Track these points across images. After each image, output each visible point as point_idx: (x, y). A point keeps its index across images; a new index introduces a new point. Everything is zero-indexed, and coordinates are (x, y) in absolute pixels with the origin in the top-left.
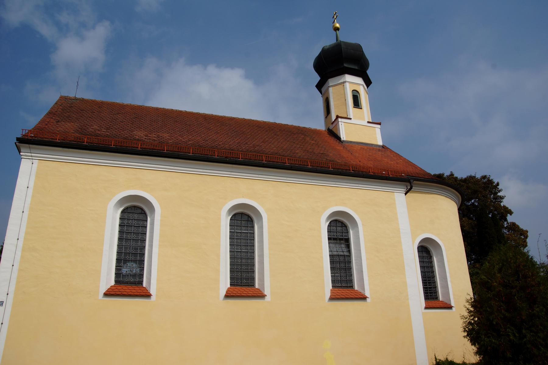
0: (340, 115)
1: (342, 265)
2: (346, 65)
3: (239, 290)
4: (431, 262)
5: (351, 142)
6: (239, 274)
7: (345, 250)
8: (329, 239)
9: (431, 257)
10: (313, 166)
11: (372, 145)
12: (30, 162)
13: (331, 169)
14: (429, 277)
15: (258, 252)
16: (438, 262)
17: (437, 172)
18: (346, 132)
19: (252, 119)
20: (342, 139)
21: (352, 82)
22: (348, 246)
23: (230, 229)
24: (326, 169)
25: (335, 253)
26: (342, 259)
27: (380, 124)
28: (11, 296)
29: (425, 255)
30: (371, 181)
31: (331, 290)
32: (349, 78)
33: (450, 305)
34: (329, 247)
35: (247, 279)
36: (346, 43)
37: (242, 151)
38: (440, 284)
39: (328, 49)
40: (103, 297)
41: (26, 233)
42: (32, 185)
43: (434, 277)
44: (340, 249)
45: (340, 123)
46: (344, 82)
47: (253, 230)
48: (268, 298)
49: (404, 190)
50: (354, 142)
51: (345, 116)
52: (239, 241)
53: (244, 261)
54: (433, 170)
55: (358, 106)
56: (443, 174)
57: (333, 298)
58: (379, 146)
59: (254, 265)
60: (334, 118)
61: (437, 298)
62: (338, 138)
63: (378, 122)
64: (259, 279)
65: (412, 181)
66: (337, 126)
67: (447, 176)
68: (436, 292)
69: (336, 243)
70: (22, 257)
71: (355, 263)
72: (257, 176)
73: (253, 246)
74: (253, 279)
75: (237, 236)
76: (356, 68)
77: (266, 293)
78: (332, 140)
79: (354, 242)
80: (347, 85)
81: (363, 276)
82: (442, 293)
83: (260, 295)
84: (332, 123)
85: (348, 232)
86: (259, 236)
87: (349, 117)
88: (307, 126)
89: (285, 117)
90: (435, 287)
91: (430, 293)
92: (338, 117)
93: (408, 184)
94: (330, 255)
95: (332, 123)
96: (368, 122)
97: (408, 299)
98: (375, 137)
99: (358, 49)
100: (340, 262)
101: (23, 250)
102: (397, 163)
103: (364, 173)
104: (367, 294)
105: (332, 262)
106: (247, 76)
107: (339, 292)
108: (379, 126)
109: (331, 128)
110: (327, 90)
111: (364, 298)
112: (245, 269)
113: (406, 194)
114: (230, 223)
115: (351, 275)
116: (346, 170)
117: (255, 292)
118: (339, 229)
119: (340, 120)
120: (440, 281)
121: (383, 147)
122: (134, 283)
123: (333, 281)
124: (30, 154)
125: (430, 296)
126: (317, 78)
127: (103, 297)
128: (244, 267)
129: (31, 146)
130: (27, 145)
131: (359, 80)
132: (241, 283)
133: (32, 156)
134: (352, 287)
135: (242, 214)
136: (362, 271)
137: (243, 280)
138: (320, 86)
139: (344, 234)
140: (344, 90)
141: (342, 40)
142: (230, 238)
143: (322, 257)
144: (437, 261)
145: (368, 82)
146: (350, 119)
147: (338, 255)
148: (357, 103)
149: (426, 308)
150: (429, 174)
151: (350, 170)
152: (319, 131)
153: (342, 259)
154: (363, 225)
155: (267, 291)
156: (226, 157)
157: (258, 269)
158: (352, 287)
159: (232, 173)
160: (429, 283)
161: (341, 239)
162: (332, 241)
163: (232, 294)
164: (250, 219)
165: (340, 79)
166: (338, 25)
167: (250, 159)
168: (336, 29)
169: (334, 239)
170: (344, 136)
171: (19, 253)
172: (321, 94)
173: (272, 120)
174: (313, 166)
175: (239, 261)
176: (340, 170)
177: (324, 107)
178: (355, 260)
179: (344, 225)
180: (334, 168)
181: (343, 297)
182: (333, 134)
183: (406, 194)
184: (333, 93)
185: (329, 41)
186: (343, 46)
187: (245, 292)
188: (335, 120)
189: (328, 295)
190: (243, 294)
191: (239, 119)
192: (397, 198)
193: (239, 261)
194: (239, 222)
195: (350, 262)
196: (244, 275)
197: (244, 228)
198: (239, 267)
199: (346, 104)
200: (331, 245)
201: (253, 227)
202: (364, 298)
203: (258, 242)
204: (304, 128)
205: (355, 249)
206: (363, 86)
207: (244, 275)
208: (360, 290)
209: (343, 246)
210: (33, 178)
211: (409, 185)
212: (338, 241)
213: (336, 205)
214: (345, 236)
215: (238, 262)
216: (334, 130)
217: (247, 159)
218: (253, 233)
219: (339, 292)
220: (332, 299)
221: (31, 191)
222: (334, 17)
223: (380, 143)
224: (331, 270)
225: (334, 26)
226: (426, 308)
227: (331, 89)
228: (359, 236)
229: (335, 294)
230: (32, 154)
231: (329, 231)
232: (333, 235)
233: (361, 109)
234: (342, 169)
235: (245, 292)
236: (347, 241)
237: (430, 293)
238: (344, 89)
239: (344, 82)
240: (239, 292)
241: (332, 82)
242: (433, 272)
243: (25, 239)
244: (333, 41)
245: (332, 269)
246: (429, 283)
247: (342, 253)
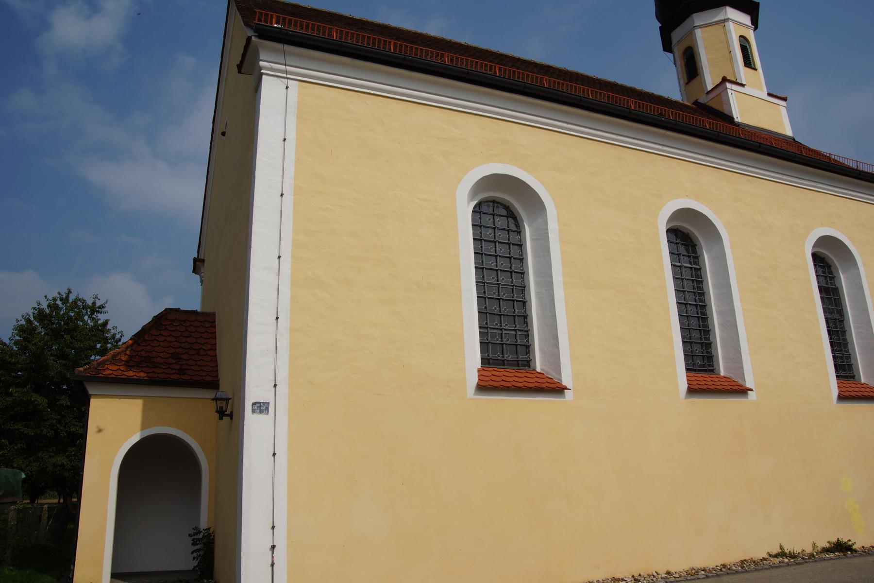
12: (280, 84)
20: (736, 120)
27: (785, 99)
28: (283, 389)
32: (731, 13)
40: (475, 394)
41: (295, 244)
42: (292, 135)
45: (729, 91)
51: (734, 79)
57: (483, 388)
63: (782, 96)
70: (294, 299)
71: (856, 334)
80: (731, 25)
87: (738, 81)
101: (294, 284)
104: (566, 382)
108: (783, 103)
111: (558, 390)
119: (728, 85)
122: (517, 364)
124: (284, 67)
127: (475, 394)
129: (289, 48)
130: (280, 46)
131: (746, 19)
133: (286, 72)
134: (853, 377)
137: (510, 358)
145: (755, 22)
146: (743, 85)
148: (748, 62)
158: (528, 363)
171: (286, 291)
189: (473, 379)
199: (731, 58)
202: (558, 390)
208: (553, 375)
210: (292, 120)
221: (291, 146)
227: (699, 33)
230: (289, 68)
238: (726, 33)
243: (293, 257)
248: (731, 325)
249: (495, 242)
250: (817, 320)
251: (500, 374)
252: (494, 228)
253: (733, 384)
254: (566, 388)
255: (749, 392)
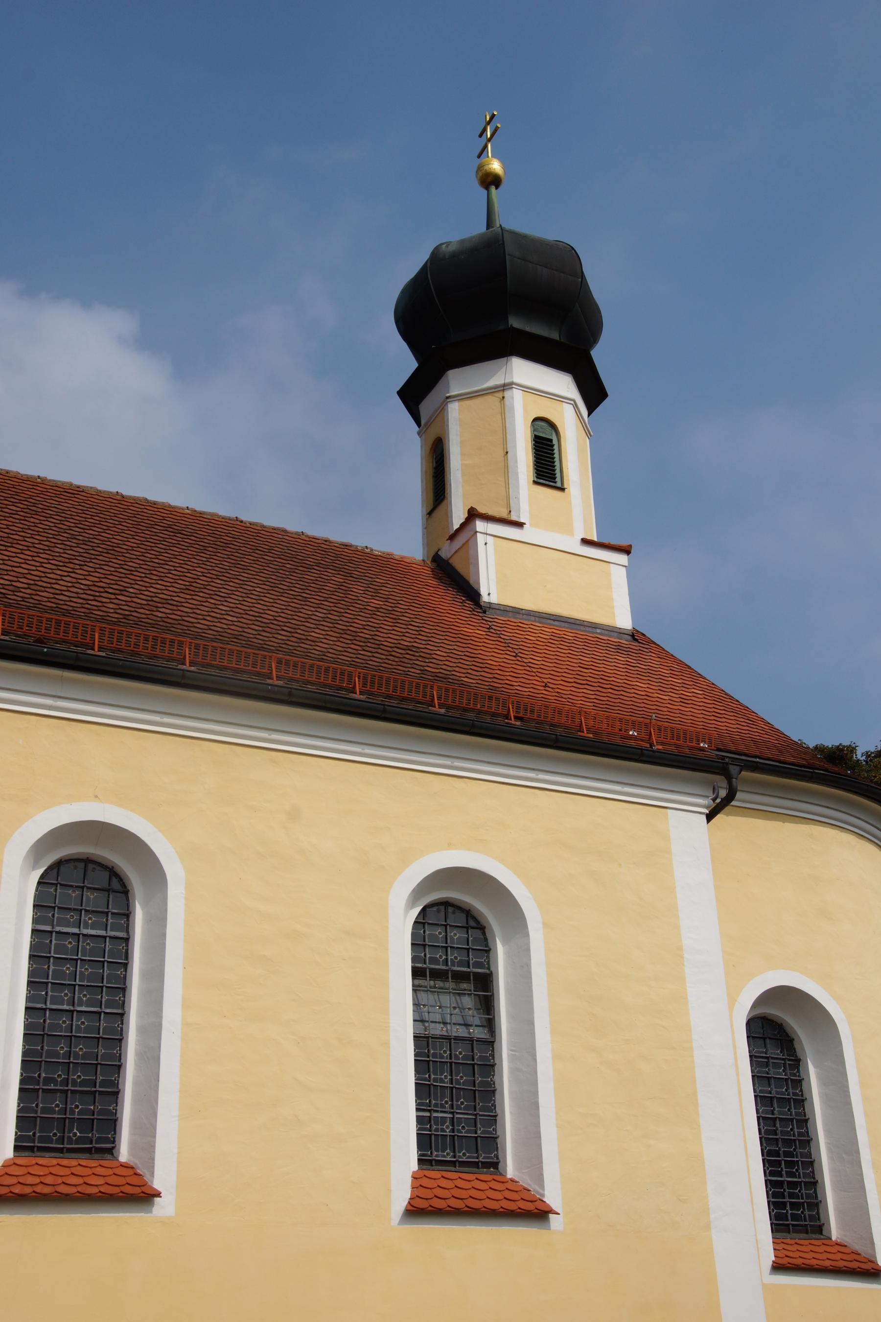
0: (481, 509)
1: (462, 1078)
2: (515, 323)
3: (50, 1168)
4: (798, 1082)
5: (517, 611)
6: (57, 1103)
7: (476, 1018)
8: (417, 973)
9: (796, 1063)
10: (370, 694)
11: (594, 626)
13: (436, 709)
14: (788, 1143)
15: (140, 1016)
16: (824, 1082)
17: (830, 741)
18: (502, 573)
19: (151, 498)
20: (485, 598)
21: (535, 388)
22: (487, 1006)
23: (35, 921)
24: (420, 707)
25: (437, 1030)
26: (460, 1051)
27: (626, 550)
29: (774, 1052)
30: (541, 757)
31: (415, 1177)
32: (522, 371)
33: (873, 1262)
34: (416, 1004)
35: (87, 1124)
36: (521, 240)
37: (102, 620)
38: (832, 1170)
39: (455, 255)
43: (807, 1141)
44: (455, 1009)
45: (480, 538)
46: (507, 387)
47: (128, 928)
48: (164, 1207)
49: (703, 803)
50: (529, 613)
51: (502, 513)
52: (68, 968)
53: (80, 1049)
54: (813, 731)
55: (553, 478)
56: (852, 749)
58: (620, 632)
59: (118, 1067)
60: (458, 517)
61: (818, 1228)
62: (471, 594)
64: (136, 1125)
65: (734, 769)
66: (469, 549)
67: (867, 754)
68: (816, 1204)
69: (442, 991)
71: (512, 1071)
72: (264, 735)
73: (123, 990)
74: (112, 1123)
75: (60, 948)
76: (555, 335)
77: (157, 1185)
78: (447, 601)
79: (508, 991)
80: (517, 397)
81: (538, 1125)
82: (838, 1211)
83: (137, 1194)
84: (452, 537)
85: (487, 950)
86: (146, 975)
87: (514, 517)
88: (359, 540)
89: (272, 502)
90: (814, 1184)
91: (794, 1206)
92: (473, 515)
93: (721, 782)
94: (416, 1037)
95: (452, 537)
96: (586, 542)
97: (708, 1227)
98: (608, 597)
99: (565, 263)
100: (453, 1067)
102: (683, 701)
103: (560, 731)
104: (552, 1197)
105: (422, 1065)
106: (146, 341)
107: (444, 1183)
108: (623, 559)
109: (445, 554)
110: (441, 412)
111: (539, 1214)
112: (84, 1083)
113: (710, 817)
114: (37, 897)
115: (493, 1119)
116: (494, 715)
117: (113, 1180)
118: (456, 935)
119: (480, 525)
120: (831, 1158)
121: (635, 635)
123: (424, 1141)
125: (795, 1217)
126: (404, 362)
128: (78, 1076)
131: (562, 384)
132: (61, 1140)
135: (87, 863)
136: (536, 1106)
138: (415, 394)
139: (472, 959)
140: (503, 413)
141: (507, 226)
142: (32, 957)
143: (386, 1044)
144: (820, 1078)
145: (593, 393)
146: (519, 525)
147: (448, 1038)
148: (546, 468)
149: (778, 1267)
150: (798, 747)
151: (507, 717)
152: (401, 561)
153: (460, 1051)
154: (545, 925)
155: (162, 1178)
156: (39, 641)
157: (136, 1083)
158: (494, 1165)
159: (542, 776)
160: (790, 1164)
161: (459, 977)
162: (428, 982)
163: (17, 1190)
164: (116, 885)
165: (494, 374)
166: (496, 166)
167: (134, 654)
168: (491, 181)
169: (437, 975)
170: (490, 590)
172: (419, 424)
173: (224, 509)
174: (370, 694)
175: (62, 1048)
176: (471, 716)
177: (425, 473)
178: (512, 1059)
179: (474, 924)
180: (448, 708)
181: (459, 1204)
182: (453, 577)
183: (710, 817)
184: (460, 422)
185: (462, 226)
186: (510, 248)
187: (73, 1180)
188: (463, 526)
189: (401, 1194)
190: (63, 1189)
191: (99, 493)
192: (675, 835)
193: (62, 1048)
194: (74, 894)
195: (490, 1067)
196: (77, 1108)
197: (91, 919)
198: (59, 1075)
199: (506, 467)
200: (423, 996)
201: (127, 915)
202: (539, 1214)
203: (144, 975)
204: (346, 546)
205: (511, 1017)
206: (576, 406)
207: (77, 1108)
208: (525, 1181)
209: (468, 1002)
211: (725, 784)
212: (450, 984)
213: (450, 846)
214: (478, 965)
215: (57, 1054)
216: (457, 563)
217: (120, 651)
218: (127, 940)
219: (444, 1183)
220: (416, 1211)
222: (487, 134)
223: (624, 620)
224: (418, 1094)
225: (480, 167)
226: (778, 1267)
227: (454, 410)
228: (528, 966)
229: (428, 1194)
231: (418, 944)
232: (433, 960)
233: (562, 489)
234: (480, 712)
235: (73, 1180)
236: (484, 984)
237: (794, 1206)
238: (504, 412)
239: (507, 387)
240: (49, 1180)
241: (458, 381)
242: (805, 1122)
244: (473, 227)
245: (422, 1090)
246: (790, 1164)
247: (462, 1032)
248: (153, 1031)
249: (424, 945)
250: (187, 1005)
251: (450, 1184)
252: (446, 926)
253: (134, 1180)
254: (158, 1195)
255: (551, 1216)
